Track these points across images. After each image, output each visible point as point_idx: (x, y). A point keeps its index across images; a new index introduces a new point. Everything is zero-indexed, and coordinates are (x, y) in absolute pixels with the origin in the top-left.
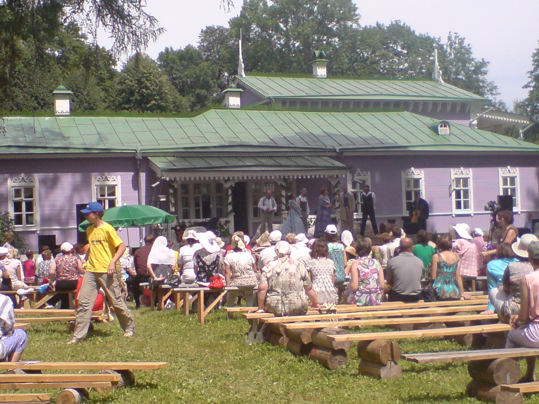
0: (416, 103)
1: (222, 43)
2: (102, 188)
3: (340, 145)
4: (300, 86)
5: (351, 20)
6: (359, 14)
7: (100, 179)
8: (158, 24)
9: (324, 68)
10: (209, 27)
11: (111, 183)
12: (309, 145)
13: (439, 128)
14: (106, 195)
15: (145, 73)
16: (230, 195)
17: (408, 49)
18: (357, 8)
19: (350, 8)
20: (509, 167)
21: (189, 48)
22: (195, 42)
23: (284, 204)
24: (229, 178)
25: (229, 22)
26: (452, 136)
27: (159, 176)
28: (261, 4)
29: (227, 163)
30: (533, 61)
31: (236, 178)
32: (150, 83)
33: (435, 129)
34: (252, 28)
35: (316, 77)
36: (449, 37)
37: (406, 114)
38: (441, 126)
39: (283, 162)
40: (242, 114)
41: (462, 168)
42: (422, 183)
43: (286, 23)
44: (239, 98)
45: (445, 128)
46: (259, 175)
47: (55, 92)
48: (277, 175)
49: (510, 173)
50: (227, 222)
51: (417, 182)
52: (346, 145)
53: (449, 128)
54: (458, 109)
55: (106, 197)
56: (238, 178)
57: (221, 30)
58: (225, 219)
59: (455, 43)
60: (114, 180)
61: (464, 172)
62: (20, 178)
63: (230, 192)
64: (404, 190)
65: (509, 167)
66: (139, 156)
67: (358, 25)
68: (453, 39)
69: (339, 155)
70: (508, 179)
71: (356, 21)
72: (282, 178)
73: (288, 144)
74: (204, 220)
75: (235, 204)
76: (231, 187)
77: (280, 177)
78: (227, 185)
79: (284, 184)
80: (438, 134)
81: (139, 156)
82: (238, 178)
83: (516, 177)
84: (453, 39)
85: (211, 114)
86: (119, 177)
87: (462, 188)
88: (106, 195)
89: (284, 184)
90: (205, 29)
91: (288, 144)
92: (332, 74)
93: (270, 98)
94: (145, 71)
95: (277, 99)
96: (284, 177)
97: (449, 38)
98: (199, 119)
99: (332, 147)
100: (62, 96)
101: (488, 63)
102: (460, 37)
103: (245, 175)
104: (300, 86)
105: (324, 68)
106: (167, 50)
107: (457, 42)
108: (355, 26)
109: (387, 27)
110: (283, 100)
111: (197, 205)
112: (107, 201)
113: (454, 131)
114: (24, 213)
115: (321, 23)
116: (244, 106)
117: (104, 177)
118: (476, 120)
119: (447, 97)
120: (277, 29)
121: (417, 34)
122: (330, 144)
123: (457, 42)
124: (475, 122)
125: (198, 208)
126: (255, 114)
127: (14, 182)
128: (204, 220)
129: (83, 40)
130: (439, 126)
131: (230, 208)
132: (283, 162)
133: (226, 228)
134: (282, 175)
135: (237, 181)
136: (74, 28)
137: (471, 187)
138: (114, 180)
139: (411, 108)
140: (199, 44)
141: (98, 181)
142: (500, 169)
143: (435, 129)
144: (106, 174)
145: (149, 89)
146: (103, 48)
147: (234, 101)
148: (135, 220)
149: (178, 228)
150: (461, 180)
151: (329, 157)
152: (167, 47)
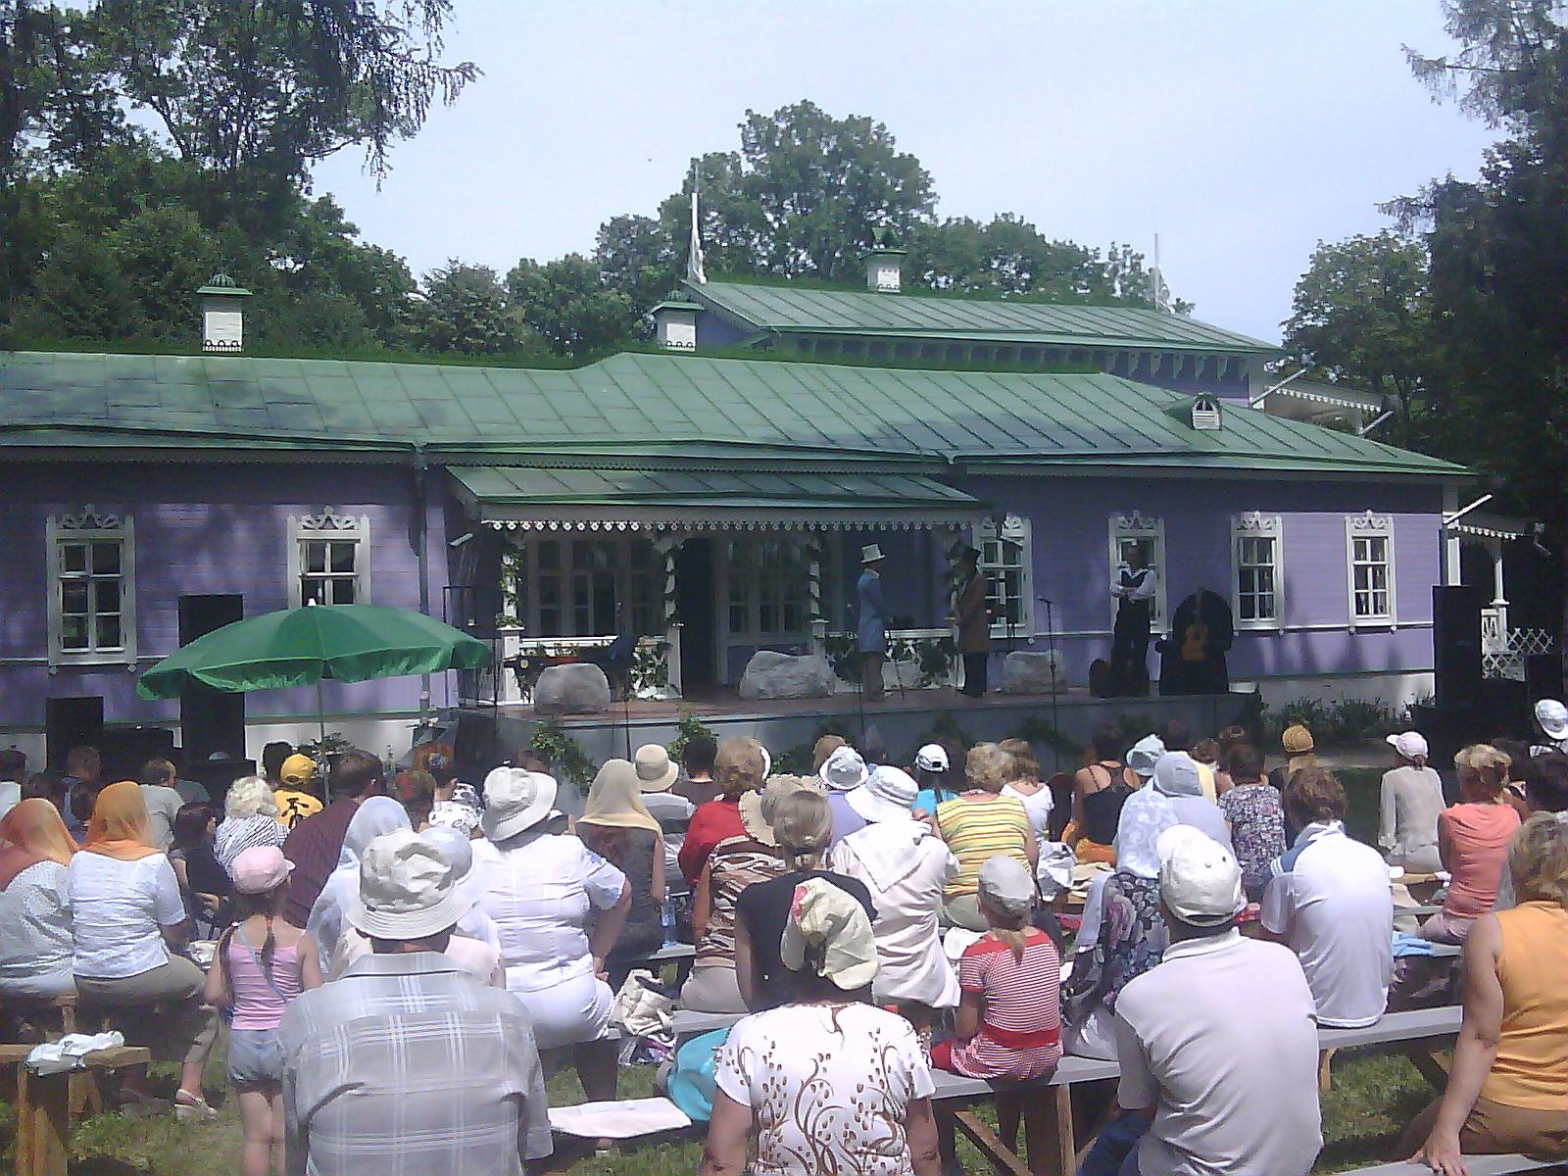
0: (1124, 354)
1: (645, 252)
2: (314, 550)
3: (955, 448)
4: (842, 308)
5: (917, 205)
6: (935, 194)
7: (309, 522)
8: (450, 14)
9: (895, 272)
10: (618, 219)
11: (339, 534)
12: (876, 445)
13: (1195, 413)
14: (328, 567)
15: (473, 300)
16: (671, 573)
17: (1032, 269)
18: (932, 180)
19: (917, 180)
20: (1369, 512)
21: (572, 263)
22: (587, 248)
23: (817, 600)
24: (668, 527)
25: (659, 209)
26: (1225, 432)
27: (473, 516)
28: (728, 168)
29: (663, 487)
30: (1296, 300)
31: (687, 528)
32: (485, 324)
33: (1184, 417)
34: (708, 219)
35: (875, 290)
36: (1110, 253)
37: (1102, 377)
38: (1200, 408)
39: (812, 486)
40: (702, 367)
41: (1257, 513)
42: (1277, 548)
43: (779, 210)
44: (693, 328)
45: (1209, 413)
46: (751, 521)
47: (203, 290)
48: (800, 520)
49: (1373, 528)
50: (662, 648)
51: (1266, 544)
52: (971, 447)
53: (1220, 413)
54: (1222, 370)
55: (328, 573)
56: (694, 526)
57: (642, 223)
58: (656, 640)
59: (1124, 266)
60: (352, 528)
61: (1263, 523)
62: (81, 516)
63: (670, 566)
64: (1236, 561)
65: (1369, 512)
66: (421, 462)
67: (932, 216)
68: (1120, 256)
69: (955, 471)
70: (1368, 542)
71: (929, 210)
72: (812, 528)
73: (823, 443)
74: (598, 641)
75: (682, 596)
76: (673, 552)
77: (806, 525)
78: (664, 546)
79: (816, 545)
80: (1193, 428)
81: (421, 462)
82: (694, 526)
83: (1275, 539)
84: (1120, 256)
85: (623, 365)
86: (365, 521)
87: (1369, 562)
88: (328, 567)
89: (816, 545)
90: (608, 223)
91: (823, 443)
92: (913, 285)
93: (769, 330)
94: (472, 294)
95: (787, 332)
96: (818, 526)
97: (1112, 256)
98: (589, 373)
99: (936, 451)
100: (224, 302)
101: (1192, 305)
102: (1134, 253)
103: (713, 521)
104: (842, 308)
105: (895, 272)
106: (524, 261)
107: (1128, 264)
108: (925, 218)
109: (987, 227)
110: (804, 337)
111: (580, 597)
112: (329, 584)
113: (1229, 421)
114: (93, 615)
115: (855, 213)
116: (702, 349)
117: (323, 518)
118: (1262, 402)
119: (1194, 343)
120: (763, 226)
121: (1049, 241)
122: (930, 446)
123: (1128, 264)
124: (1260, 405)
125: (580, 606)
126: (737, 370)
127: (65, 527)
128: (598, 641)
129: (348, 236)
130: (1195, 408)
131: (670, 609)
132: (812, 486)
133: (658, 663)
134: (812, 520)
135: (690, 536)
136: (328, 210)
137: (1025, 562)
138: (352, 528)
139: (1112, 364)
140: (596, 254)
141: (305, 528)
142: (1347, 517)
143: (1184, 417)
144: (329, 510)
145: (483, 337)
146: (390, 253)
147: (680, 334)
148: (335, 661)
149: (524, 664)
150: (1255, 543)
151: (929, 477)
152: (523, 257)
